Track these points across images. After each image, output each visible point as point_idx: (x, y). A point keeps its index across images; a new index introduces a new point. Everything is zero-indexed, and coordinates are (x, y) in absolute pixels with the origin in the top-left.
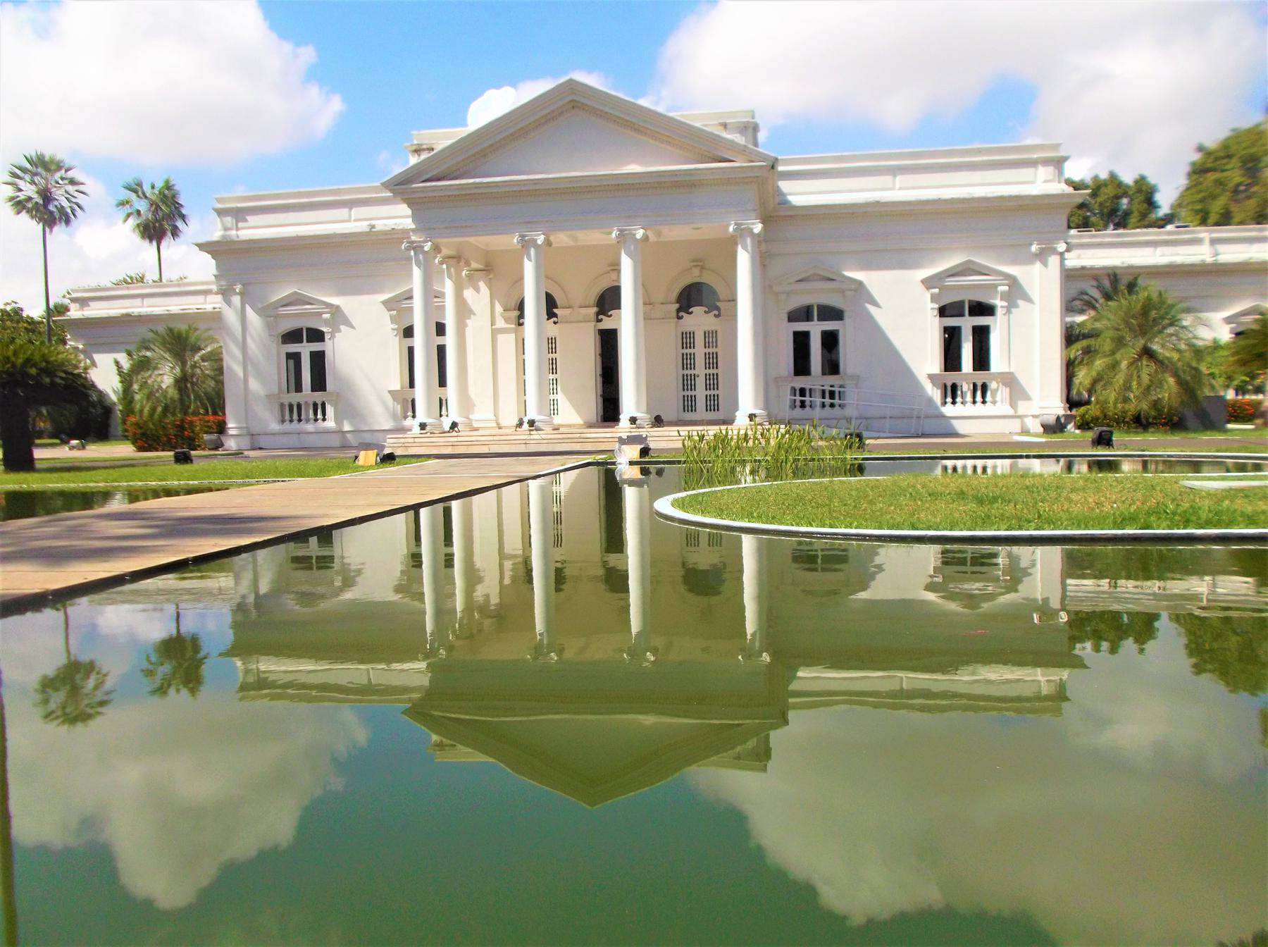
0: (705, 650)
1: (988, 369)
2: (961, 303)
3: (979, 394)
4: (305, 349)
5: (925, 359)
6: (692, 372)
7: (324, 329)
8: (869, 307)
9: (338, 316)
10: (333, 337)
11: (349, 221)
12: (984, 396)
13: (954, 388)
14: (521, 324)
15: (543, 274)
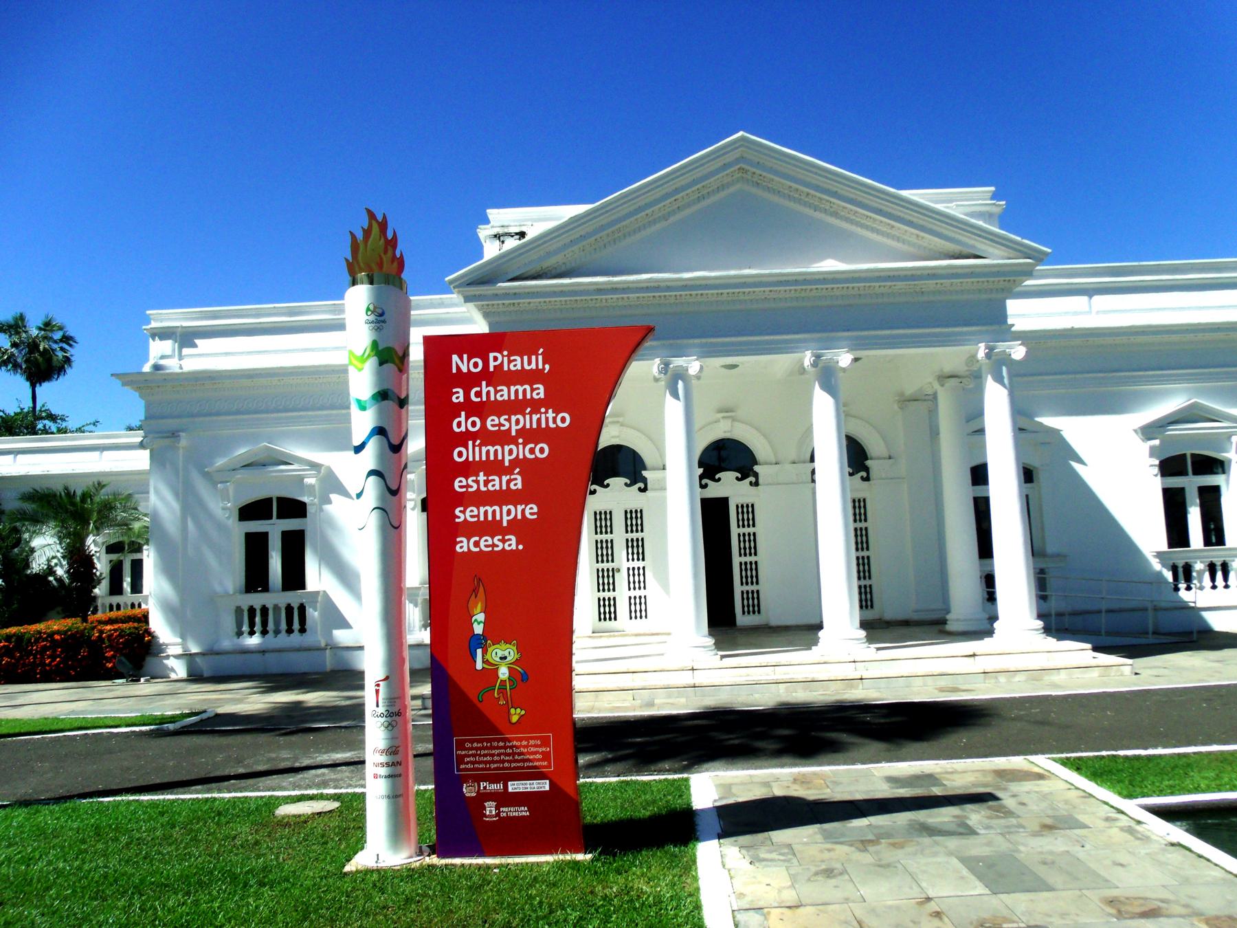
1: (1188, 545)
2: (268, 501)
3: (1219, 575)
4: (275, 528)
5: (1147, 532)
6: (610, 565)
7: (305, 499)
8: (1074, 464)
12: (1226, 578)
13: (1188, 569)
14: (813, 481)
15: (844, 413)
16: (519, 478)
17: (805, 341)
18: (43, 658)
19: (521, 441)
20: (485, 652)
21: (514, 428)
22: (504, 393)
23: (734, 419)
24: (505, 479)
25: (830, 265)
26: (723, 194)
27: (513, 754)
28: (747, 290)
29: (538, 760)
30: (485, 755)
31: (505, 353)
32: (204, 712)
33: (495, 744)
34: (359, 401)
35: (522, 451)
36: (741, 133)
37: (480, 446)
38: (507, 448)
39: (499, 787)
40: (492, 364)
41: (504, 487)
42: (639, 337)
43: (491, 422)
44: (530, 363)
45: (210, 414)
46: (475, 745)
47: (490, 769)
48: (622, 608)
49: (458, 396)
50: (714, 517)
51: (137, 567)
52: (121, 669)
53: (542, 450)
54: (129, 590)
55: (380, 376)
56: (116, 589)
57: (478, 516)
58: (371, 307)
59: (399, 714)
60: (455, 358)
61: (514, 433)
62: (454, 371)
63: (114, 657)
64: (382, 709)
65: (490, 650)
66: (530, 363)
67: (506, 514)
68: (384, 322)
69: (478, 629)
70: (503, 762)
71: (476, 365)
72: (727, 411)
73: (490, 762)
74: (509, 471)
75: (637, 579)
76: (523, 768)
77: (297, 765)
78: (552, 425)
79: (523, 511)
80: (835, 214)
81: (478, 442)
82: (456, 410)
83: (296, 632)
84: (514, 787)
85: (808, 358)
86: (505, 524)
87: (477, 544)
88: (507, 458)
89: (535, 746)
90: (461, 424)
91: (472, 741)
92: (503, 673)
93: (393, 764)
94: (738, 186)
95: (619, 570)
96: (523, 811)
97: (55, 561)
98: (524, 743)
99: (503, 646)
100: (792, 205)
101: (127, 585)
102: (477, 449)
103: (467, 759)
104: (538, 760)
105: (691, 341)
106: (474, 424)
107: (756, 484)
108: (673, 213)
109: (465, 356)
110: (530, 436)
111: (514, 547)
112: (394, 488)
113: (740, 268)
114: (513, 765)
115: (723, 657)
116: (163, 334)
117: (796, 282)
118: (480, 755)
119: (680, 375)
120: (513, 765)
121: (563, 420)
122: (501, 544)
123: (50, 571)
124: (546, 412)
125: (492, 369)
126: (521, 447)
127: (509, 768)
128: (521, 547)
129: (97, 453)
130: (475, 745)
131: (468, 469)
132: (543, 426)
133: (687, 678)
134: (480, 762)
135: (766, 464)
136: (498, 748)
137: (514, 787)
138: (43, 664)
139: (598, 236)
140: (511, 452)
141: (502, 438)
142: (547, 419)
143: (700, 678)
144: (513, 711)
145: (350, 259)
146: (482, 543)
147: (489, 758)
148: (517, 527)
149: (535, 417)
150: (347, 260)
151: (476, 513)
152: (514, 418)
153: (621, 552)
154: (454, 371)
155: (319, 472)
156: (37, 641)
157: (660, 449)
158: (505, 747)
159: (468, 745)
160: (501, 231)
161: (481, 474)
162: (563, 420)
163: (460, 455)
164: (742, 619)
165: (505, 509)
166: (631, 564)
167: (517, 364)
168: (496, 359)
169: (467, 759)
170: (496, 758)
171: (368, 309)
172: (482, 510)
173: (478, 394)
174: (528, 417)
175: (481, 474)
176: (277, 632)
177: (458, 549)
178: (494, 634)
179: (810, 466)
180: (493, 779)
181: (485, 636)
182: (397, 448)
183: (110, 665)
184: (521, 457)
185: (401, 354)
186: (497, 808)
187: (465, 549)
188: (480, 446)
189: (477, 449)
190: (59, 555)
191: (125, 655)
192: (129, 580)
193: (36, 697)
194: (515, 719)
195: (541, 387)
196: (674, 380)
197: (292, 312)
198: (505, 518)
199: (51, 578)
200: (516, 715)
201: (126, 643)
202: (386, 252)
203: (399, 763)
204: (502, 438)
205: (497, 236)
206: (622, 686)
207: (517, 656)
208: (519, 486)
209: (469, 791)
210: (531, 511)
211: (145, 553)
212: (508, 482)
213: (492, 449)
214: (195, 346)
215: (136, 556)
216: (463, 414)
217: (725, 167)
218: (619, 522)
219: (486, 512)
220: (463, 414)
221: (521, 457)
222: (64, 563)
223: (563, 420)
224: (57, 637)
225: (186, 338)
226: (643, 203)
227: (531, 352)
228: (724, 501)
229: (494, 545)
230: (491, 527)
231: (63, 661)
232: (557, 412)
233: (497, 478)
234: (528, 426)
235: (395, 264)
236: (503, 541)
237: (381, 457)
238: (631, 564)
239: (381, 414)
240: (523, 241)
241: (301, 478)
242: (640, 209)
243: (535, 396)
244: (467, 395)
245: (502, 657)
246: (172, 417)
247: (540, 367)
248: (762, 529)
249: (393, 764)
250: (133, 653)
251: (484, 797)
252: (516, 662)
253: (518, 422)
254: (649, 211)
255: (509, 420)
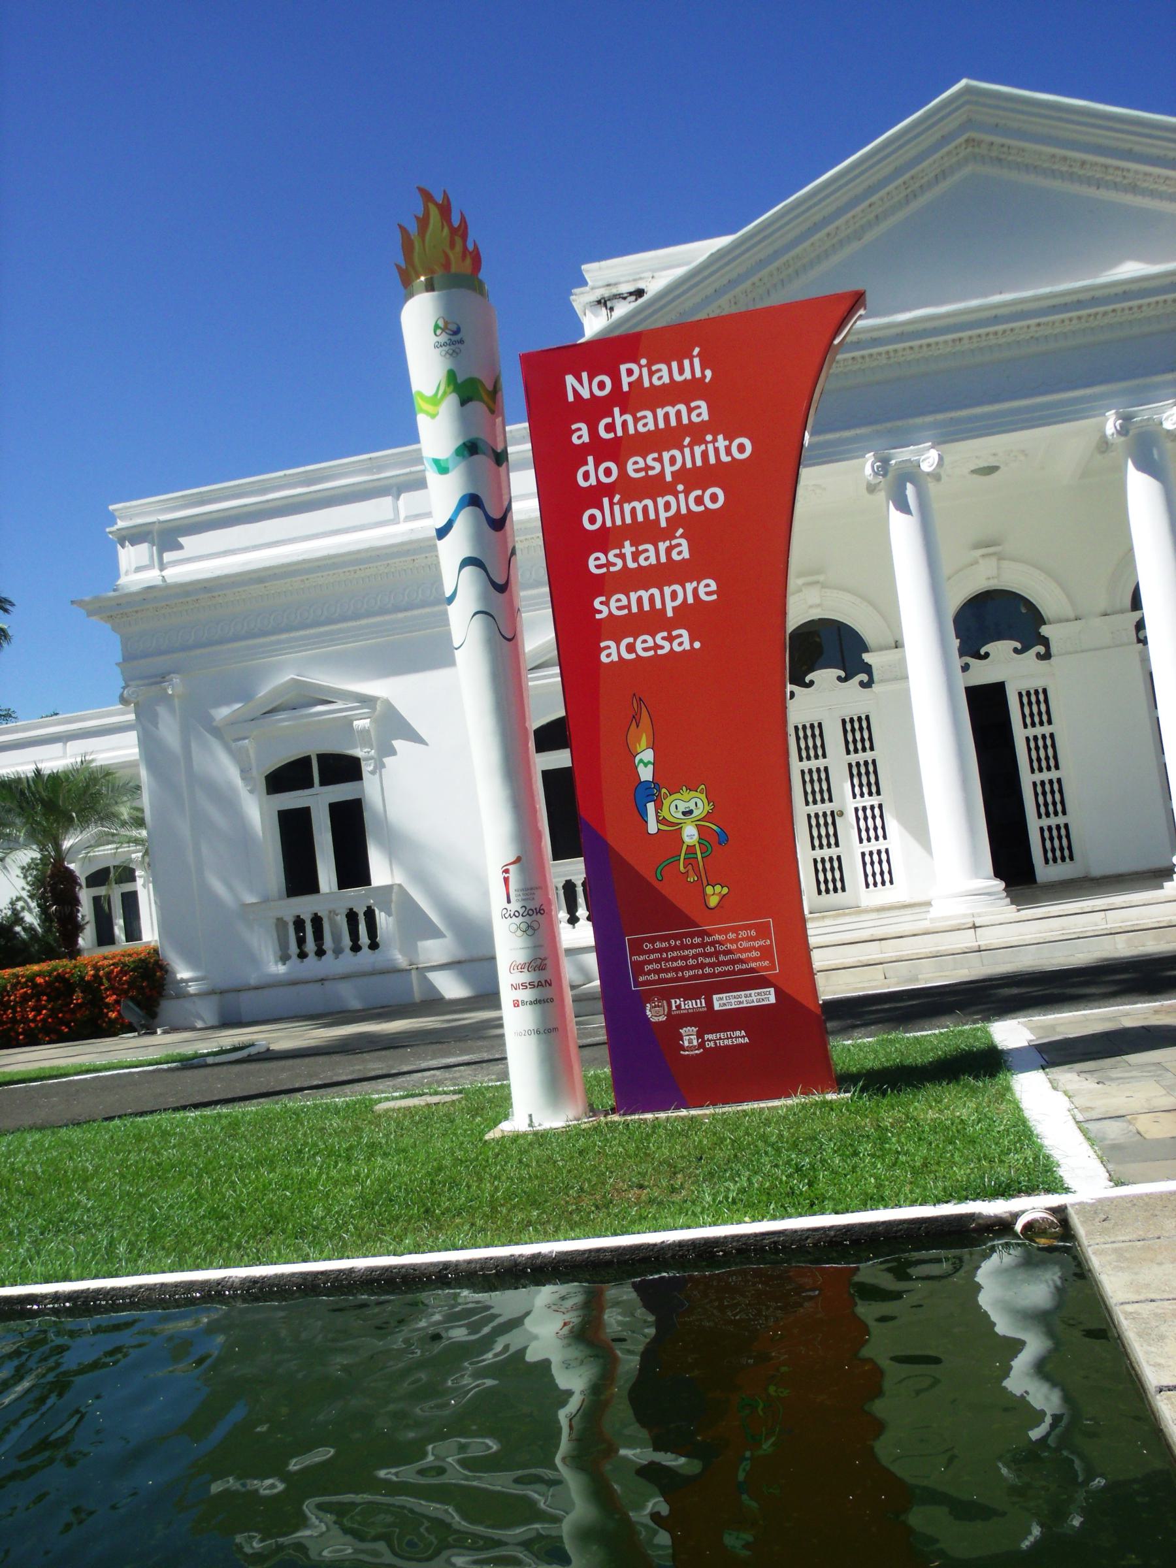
0: (1086, 1377)
2: (305, 762)
4: (318, 800)
6: (827, 807)
7: (359, 752)
9: (394, 727)
10: (380, 766)
11: (395, 521)
14: (1143, 641)
16: (684, 542)
17: (1102, 396)
18: (24, 1010)
19: (680, 487)
20: (659, 807)
21: (669, 470)
22: (648, 422)
23: (1001, 557)
24: (662, 546)
25: (1130, 269)
26: (944, 186)
27: (716, 954)
28: (1000, 328)
29: (755, 960)
30: (674, 959)
31: (643, 362)
32: (253, 1045)
33: (688, 941)
34: (436, 462)
35: (686, 503)
36: (964, 82)
37: (621, 503)
38: (661, 501)
39: (699, 1004)
40: (625, 381)
41: (663, 559)
42: (844, 307)
43: (634, 466)
44: (681, 371)
45: (211, 643)
46: (658, 945)
47: (683, 979)
48: (854, 872)
49: (581, 434)
50: (987, 712)
51: (130, 902)
52: (129, 1018)
53: (714, 498)
54: (123, 937)
55: (464, 421)
56: (105, 936)
57: (629, 607)
58: (441, 323)
59: (540, 911)
60: (570, 380)
61: (669, 478)
62: (571, 398)
63: (117, 1002)
64: (515, 906)
65: (666, 803)
66: (681, 371)
67: (670, 598)
68: (461, 342)
69: (646, 774)
70: (702, 966)
71: (602, 386)
72: (988, 544)
73: (681, 969)
74: (668, 534)
75: (872, 824)
76: (733, 973)
77: (394, 1071)
78: (725, 458)
79: (695, 591)
80: (1134, 189)
81: (617, 498)
82: (579, 455)
83: (365, 949)
84: (722, 1002)
85: (1111, 424)
86: (670, 614)
87: (631, 648)
88: (663, 516)
89: (749, 939)
90: (590, 474)
91: (652, 940)
92: (690, 834)
93: (540, 984)
94: (968, 170)
95: (841, 814)
96: (739, 1037)
97: (20, 904)
98: (732, 936)
99: (686, 794)
100: (1057, 184)
101: (119, 931)
102: (617, 508)
103: (647, 968)
104: (755, 960)
105: (919, 421)
106: (608, 472)
107: (1047, 656)
108: (870, 225)
109: (585, 375)
110: (693, 478)
111: (687, 646)
112: (500, 581)
113: (985, 295)
114: (718, 969)
115: (1019, 910)
116: (135, 536)
117: (1080, 304)
118: (667, 960)
119: (910, 474)
120: (718, 969)
121: (742, 448)
122: (666, 644)
123: (17, 918)
124: (715, 440)
125: (626, 388)
126: (682, 496)
127: (713, 975)
128: (697, 645)
129: (59, 745)
130: (658, 945)
131: (605, 539)
132: (712, 460)
133: (966, 940)
134: (667, 970)
135: (1060, 621)
136: (693, 946)
137: (722, 1002)
138: (25, 1020)
139: (755, 279)
140: (667, 506)
141: (653, 487)
142: (716, 450)
143: (987, 938)
144: (709, 890)
145: (403, 265)
146: (639, 646)
147: (680, 963)
148: (688, 615)
149: (698, 450)
150: (398, 267)
151: (625, 602)
152: (666, 456)
153: (842, 787)
154: (571, 398)
155: (374, 709)
156: (14, 986)
157: (890, 614)
158: (703, 945)
159: (648, 946)
160: (606, 293)
161: (627, 543)
162: (742, 448)
163: (592, 520)
164: (1044, 872)
165: (667, 591)
166: (860, 802)
167: (663, 374)
168: (630, 372)
169: (647, 968)
170: (691, 962)
171: (436, 327)
172: (634, 596)
173: (610, 428)
174: (687, 451)
175: (627, 543)
176: (338, 951)
177: (604, 659)
178: (671, 777)
179: (1136, 616)
180: (690, 993)
181: (656, 783)
182: (499, 523)
183: (113, 1015)
184: (684, 511)
185: (490, 388)
186: (700, 1035)
187: (615, 658)
188: (621, 503)
189: (617, 508)
190: (25, 894)
191: (132, 999)
192: (121, 922)
193: (21, 1057)
194: (713, 901)
195: (703, 404)
196: (899, 485)
197: (310, 480)
198: (670, 605)
199: (18, 929)
200: (714, 895)
201: (131, 983)
202: (452, 245)
203: (548, 983)
204: (653, 487)
205: (602, 302)
206: (865, 959)
207: (708, 808)
208: (686, 555)
209: (655, 1013)
210: (707, 589)
211: (140, 882)
212: (669, 550)
213: (639, 506)
214: (180, 547)
215: (127, 887)
216: (590, 459)
217: (945, 140)
218: (834, 738)
219: (640, 599)
220: (590, 459)
221: (684, 511)
222: (33, 904)
223: (741, 448)
224: (40, 980)
225: (166, 538)
226: (818, 218)
227: (682, 355)
228: (998, 689)
229: (657, 647)
230: (651, 621)
231: (53, 1013)
232: (730, 438)
233: (650, 547)
234: (689, 465)
235: (468, 261)
236: (670, 639)
237: (478, 538)
238: (860, 802)
239: (472, 475)
240: (640, 301)
241: (349, 722)
242: (816, 228)
243: (695, 419)
244: (593, 432)
245: (686, 812)
246: (160, 653)
247: (698, 374)
248: (1062, 727)
249: (540, 984)
250: (144, 992)
251: (678, 1020)
252: (708, 817)
253: (673, 461)
254: (831, 228)
255: (660, 460)
